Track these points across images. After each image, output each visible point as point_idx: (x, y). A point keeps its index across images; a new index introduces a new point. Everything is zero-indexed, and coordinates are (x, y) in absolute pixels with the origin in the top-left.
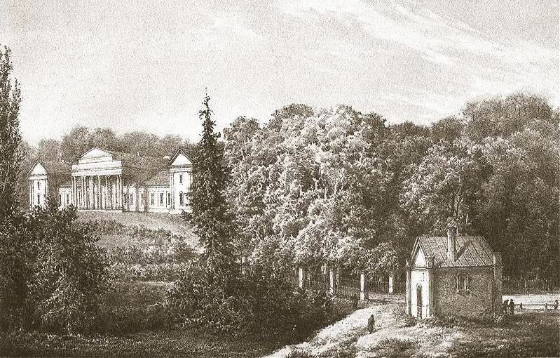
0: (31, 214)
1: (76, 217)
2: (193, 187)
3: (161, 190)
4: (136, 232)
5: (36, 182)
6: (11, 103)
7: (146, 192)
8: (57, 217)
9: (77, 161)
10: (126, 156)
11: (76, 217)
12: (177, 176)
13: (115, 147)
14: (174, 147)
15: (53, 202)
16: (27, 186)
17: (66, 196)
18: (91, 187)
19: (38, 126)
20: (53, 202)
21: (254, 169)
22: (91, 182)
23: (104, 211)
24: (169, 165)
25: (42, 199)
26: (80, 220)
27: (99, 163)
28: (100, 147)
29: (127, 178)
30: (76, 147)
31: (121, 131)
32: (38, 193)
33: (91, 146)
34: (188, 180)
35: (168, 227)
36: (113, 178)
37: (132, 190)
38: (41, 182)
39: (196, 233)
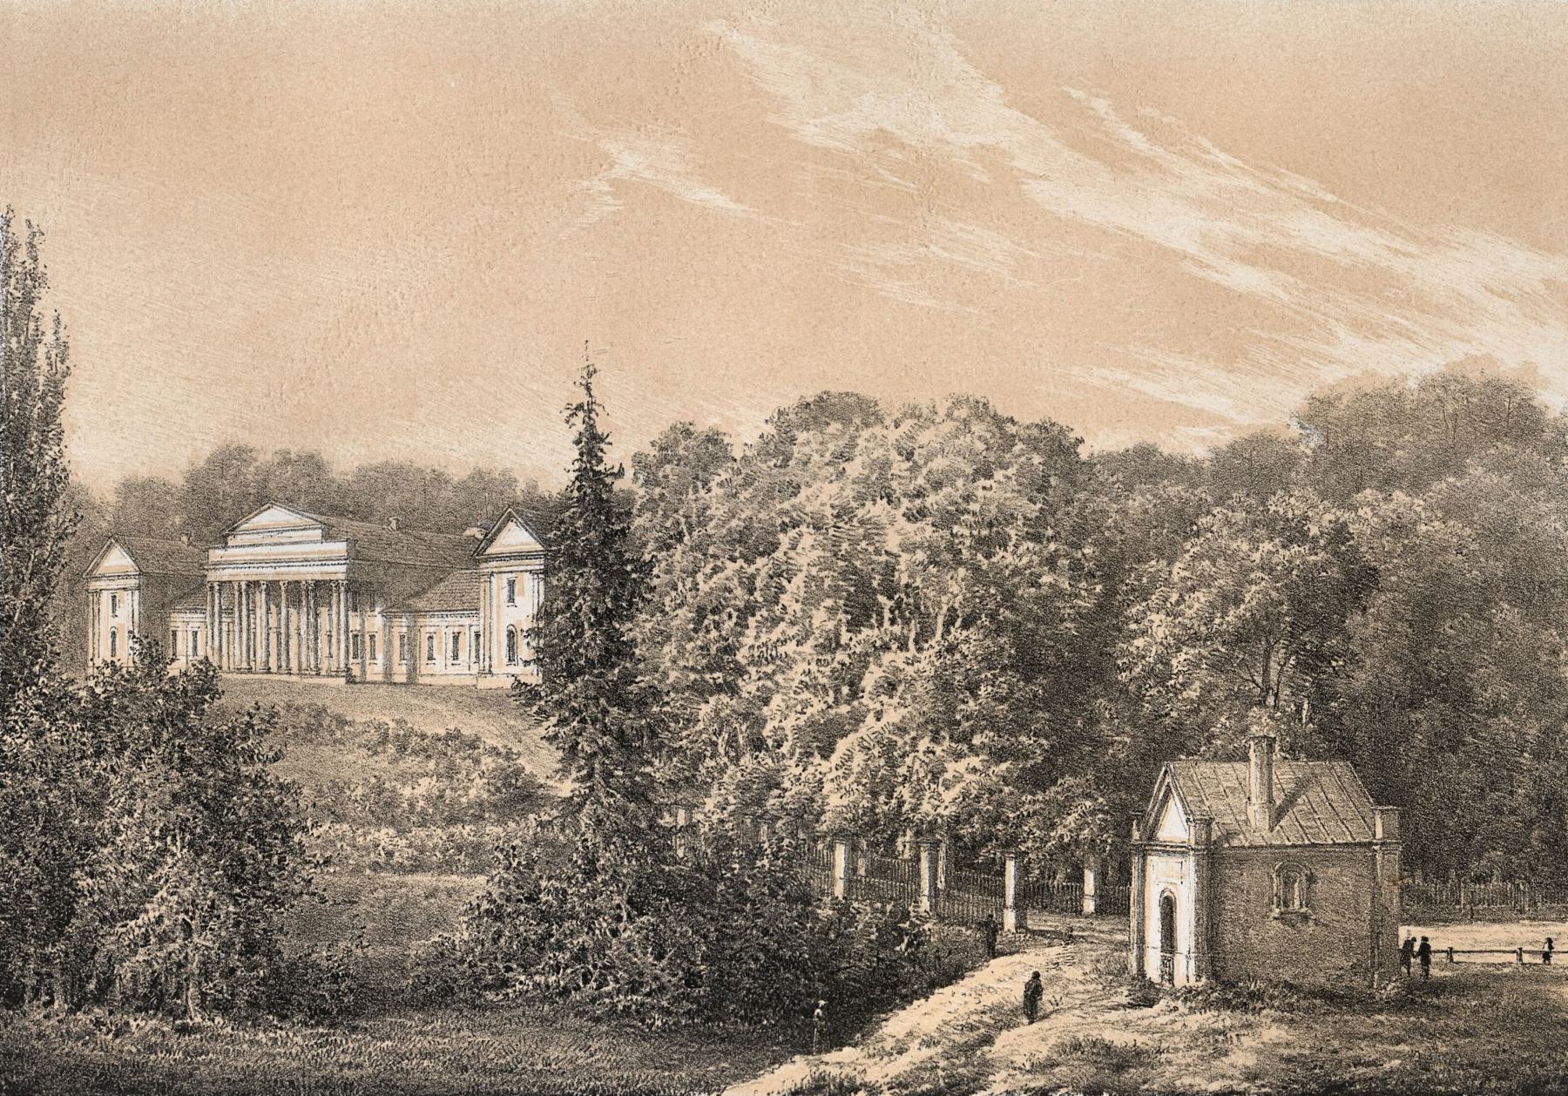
0: (91, 683)
1: (216, 694)
6: (41, 379)
11: (216, 694)
13: (331, 505)
15: (154, 652)
19: (110, 444)
20: (154, 652)
22: (261, 598)
24: (477, 554)
28: (289, 503)
29: (359, 592)
30: (219, 501)
31: (347, 457)
32: (112, 628)
33: (262, 501)
34: (531, 595)
36: (321, 590)
37: (376, 622)
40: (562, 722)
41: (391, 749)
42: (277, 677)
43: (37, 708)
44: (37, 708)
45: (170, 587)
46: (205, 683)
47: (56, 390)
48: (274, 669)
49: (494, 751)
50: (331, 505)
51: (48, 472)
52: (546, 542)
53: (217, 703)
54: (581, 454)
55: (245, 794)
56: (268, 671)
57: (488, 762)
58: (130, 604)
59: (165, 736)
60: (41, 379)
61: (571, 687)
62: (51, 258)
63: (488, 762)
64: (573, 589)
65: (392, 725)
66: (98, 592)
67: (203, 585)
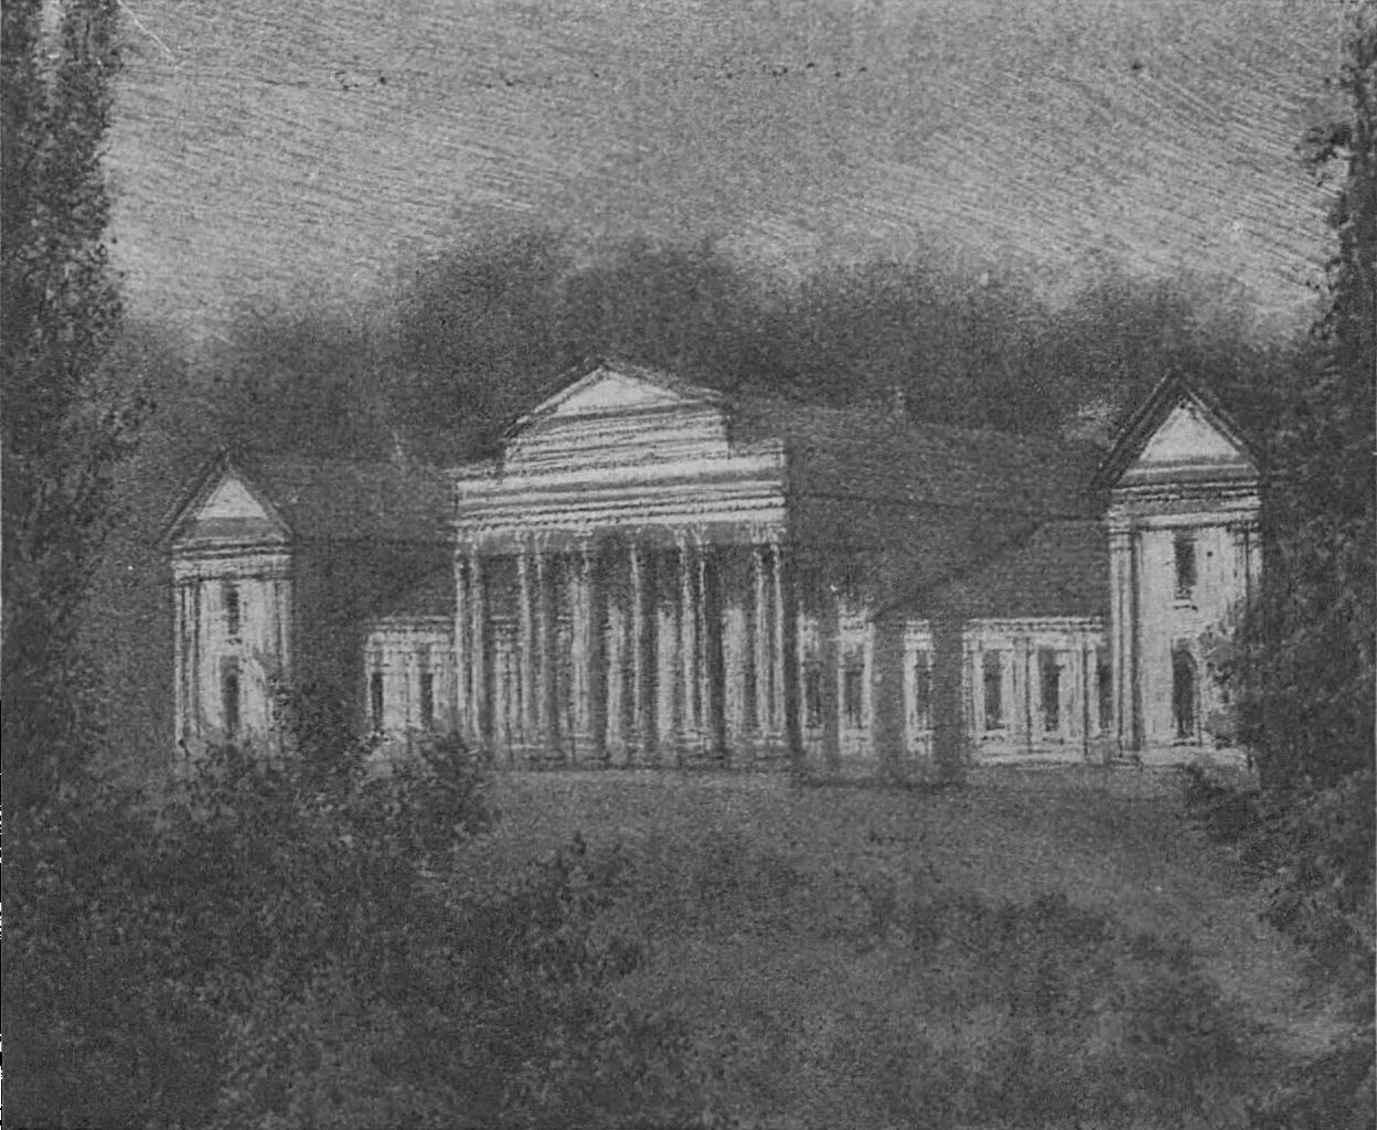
0: (182, 798)
1: (480, 818)
2: (1261, 619)
3: (1051, 635)
4: (884, 909)
5: (212, 590)
6: (50, 78)
7: (949, 649)
8: (360, 822)
9: (488, 450)
10: (818, 423)
11: (480, 818)
12: (1159, 552)
13: (739, 354)
14: (1155, 352)
15: (326, 697)
16: (158, 643)
17: (412, 676)
18: (581, 621)
19: (223, 213)
20: (326, 697)
21: (437, 215)
22: (579, 592)
23: (670, 779)
24: (1106, 471)
25: (257, 709)
26: (504, 830)
27: (631, 452)
28: (645, 357)
29: (815, 565)
30: (486, 344)
31: (778, 250)
32: (231, 643)
33: (577, 364)
34: (1228, 569)
35: (1090, 883)
36: (722, 566)
37: (855, 634)
38: (246, 589)
39: (1283, 918)
40: (1308, 878)
41: (900, 937)
42: (628, 777)
43: (54, 856)
44: (54, 856)
45: (357, 578)
46: (452, 778)
47: (87, 105)
48: (618, 758)
49: (1145, 947)
50: (739, 354)
51: (73, 298)
52: (1258, 451)
53: (483, 841)
54: (1347, 247)
55: (555, 1055)
56: (605, 762)
57: (1134, 975)
58: (264, 612)
59: (359, 922)
60: (50, 78)
61: (1330, 795)
62: (118, 212)
63: (1134, 975)
64: (1330, 564)
65: (904, 881)
66: (196, 582)
67: (444, 566)
